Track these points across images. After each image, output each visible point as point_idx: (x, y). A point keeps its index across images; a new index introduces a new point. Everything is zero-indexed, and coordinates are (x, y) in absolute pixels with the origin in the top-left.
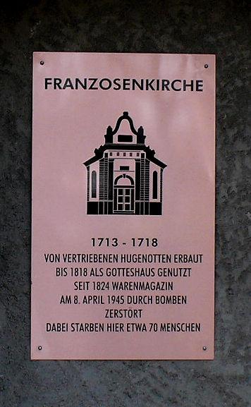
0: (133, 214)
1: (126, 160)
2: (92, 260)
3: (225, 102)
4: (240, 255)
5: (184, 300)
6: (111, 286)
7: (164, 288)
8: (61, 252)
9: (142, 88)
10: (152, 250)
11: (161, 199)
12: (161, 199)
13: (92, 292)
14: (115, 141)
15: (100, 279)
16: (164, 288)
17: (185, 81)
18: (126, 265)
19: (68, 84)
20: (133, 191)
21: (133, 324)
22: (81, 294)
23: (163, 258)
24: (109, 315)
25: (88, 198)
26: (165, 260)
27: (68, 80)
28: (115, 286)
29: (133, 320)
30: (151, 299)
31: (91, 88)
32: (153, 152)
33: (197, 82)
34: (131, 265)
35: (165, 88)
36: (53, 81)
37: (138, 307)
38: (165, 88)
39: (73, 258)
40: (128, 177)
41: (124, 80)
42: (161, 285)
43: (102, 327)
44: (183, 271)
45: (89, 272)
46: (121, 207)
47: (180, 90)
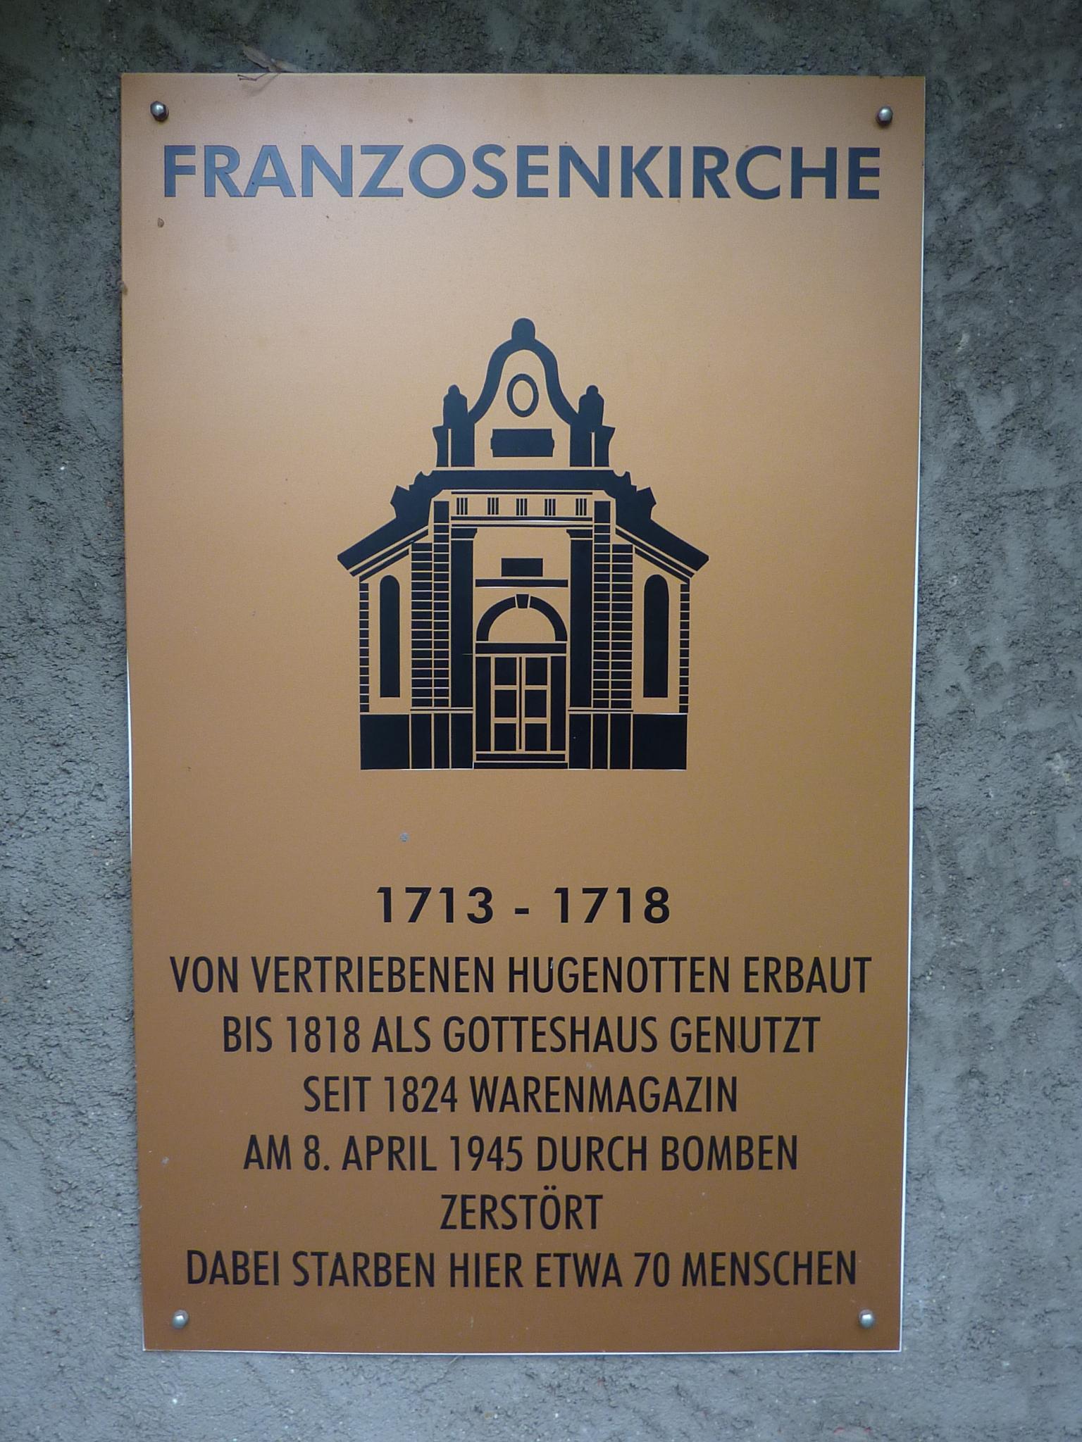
0: (564, 766)
2: (381, 982)
3: (963, 279)
4: (1019, 932)
5: (789, 1153)
6: (464, 1093)
7: (700, 1101)
8: (244, 946)
9: (601, 189)
10: (641, 939)
11: (684, 700)
12: (684, 700)
14: (485, 460)
15: (418, 1066)
16: (700, 1101)
17: (797, 153)
18: (527, 1003)
19: (269, 172)
21: (562, 1257)
22: (334, 1130)
23: (694, 974)
24: (455, 1218)
25: (364, 699)
26: (702, 982)
28: (483, 1094)
30: (643, 1151)
32: (647, 498)
34: (555, 1003)
35: (708, 186)
36: (197, 160)
37: (582, 1182)
38: (708, 186)
39: (298, 974)
40: (539, 605)
41: (524, 152)
42: (685, 1089)
43: (425, 1269)
44: (783, 1029)
45: (367, 1033)
46: (506, 735)
47: (775, 193)
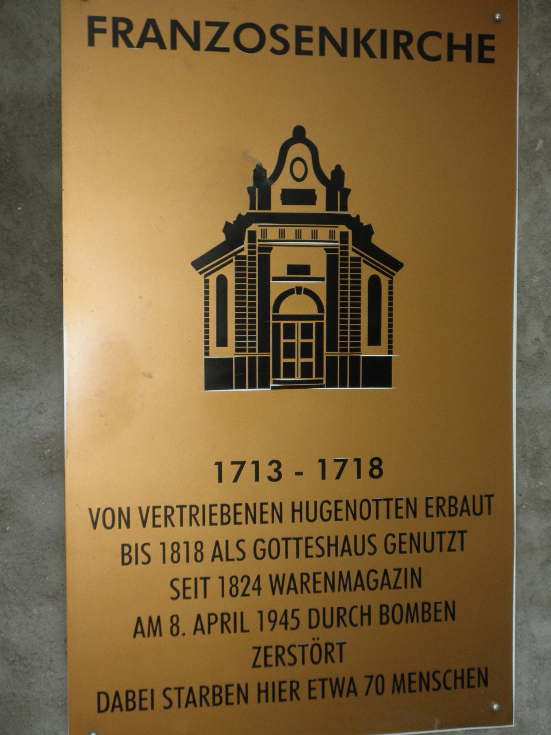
1: (297, 248)
5: (451, 611)
7: (401, 583)
9: (343, 52)
13: (217, 603)
14: (277, 206)
16: (401, 583)
17: (450, 36)
19: (151, 34)
20: (320, 327)
23: (397, 508)
24: (261, 660)
25: (207, 348)
27: (151, 23)
28: (277, 585)
29: (326, 670)
30: (369, 614)
31: (211, 47)
32: (369, 231)
33: (482, 38)
36: (108, 25)
42: (392, 575)
43: (243, 693)
44: (447, 538)
45: (208, 551)
